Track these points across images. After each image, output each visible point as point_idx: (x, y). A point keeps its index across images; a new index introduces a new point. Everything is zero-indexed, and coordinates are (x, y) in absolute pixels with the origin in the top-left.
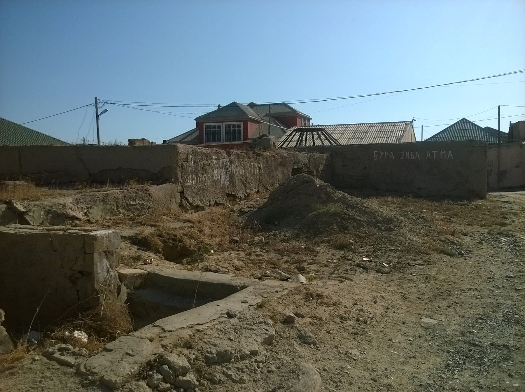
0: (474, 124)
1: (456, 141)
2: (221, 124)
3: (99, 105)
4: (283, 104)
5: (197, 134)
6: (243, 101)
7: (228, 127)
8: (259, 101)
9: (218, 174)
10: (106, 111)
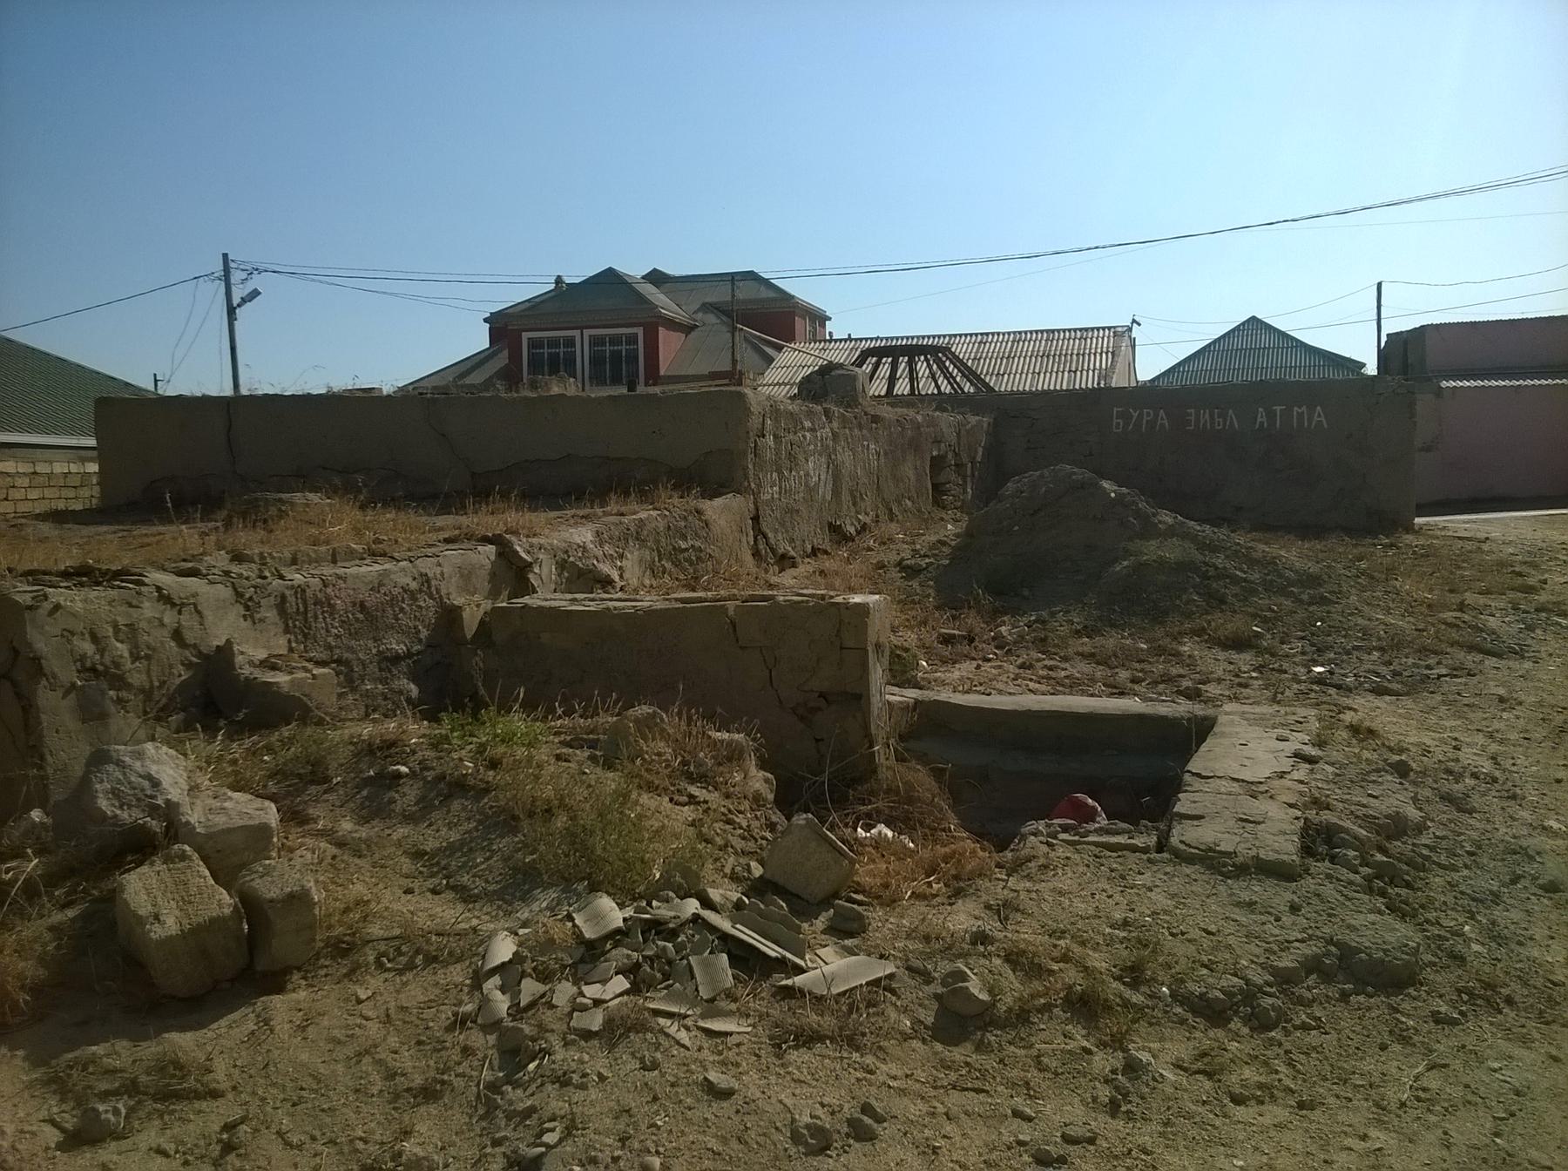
0: (1293, 338)
1: (1024, 392)
2: (577, 333)
3: (236, 276)
4: (751, 276)
5: (503, 359)
6: (634, 268)
7: (596, 341)
8: (673, 269)
9: (815, 468)
10: (255, 294)
